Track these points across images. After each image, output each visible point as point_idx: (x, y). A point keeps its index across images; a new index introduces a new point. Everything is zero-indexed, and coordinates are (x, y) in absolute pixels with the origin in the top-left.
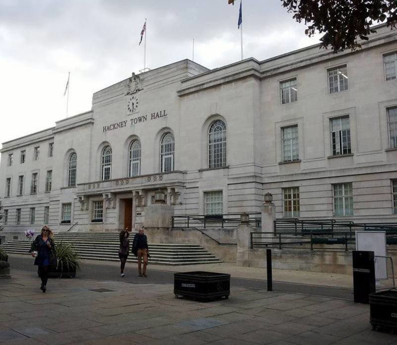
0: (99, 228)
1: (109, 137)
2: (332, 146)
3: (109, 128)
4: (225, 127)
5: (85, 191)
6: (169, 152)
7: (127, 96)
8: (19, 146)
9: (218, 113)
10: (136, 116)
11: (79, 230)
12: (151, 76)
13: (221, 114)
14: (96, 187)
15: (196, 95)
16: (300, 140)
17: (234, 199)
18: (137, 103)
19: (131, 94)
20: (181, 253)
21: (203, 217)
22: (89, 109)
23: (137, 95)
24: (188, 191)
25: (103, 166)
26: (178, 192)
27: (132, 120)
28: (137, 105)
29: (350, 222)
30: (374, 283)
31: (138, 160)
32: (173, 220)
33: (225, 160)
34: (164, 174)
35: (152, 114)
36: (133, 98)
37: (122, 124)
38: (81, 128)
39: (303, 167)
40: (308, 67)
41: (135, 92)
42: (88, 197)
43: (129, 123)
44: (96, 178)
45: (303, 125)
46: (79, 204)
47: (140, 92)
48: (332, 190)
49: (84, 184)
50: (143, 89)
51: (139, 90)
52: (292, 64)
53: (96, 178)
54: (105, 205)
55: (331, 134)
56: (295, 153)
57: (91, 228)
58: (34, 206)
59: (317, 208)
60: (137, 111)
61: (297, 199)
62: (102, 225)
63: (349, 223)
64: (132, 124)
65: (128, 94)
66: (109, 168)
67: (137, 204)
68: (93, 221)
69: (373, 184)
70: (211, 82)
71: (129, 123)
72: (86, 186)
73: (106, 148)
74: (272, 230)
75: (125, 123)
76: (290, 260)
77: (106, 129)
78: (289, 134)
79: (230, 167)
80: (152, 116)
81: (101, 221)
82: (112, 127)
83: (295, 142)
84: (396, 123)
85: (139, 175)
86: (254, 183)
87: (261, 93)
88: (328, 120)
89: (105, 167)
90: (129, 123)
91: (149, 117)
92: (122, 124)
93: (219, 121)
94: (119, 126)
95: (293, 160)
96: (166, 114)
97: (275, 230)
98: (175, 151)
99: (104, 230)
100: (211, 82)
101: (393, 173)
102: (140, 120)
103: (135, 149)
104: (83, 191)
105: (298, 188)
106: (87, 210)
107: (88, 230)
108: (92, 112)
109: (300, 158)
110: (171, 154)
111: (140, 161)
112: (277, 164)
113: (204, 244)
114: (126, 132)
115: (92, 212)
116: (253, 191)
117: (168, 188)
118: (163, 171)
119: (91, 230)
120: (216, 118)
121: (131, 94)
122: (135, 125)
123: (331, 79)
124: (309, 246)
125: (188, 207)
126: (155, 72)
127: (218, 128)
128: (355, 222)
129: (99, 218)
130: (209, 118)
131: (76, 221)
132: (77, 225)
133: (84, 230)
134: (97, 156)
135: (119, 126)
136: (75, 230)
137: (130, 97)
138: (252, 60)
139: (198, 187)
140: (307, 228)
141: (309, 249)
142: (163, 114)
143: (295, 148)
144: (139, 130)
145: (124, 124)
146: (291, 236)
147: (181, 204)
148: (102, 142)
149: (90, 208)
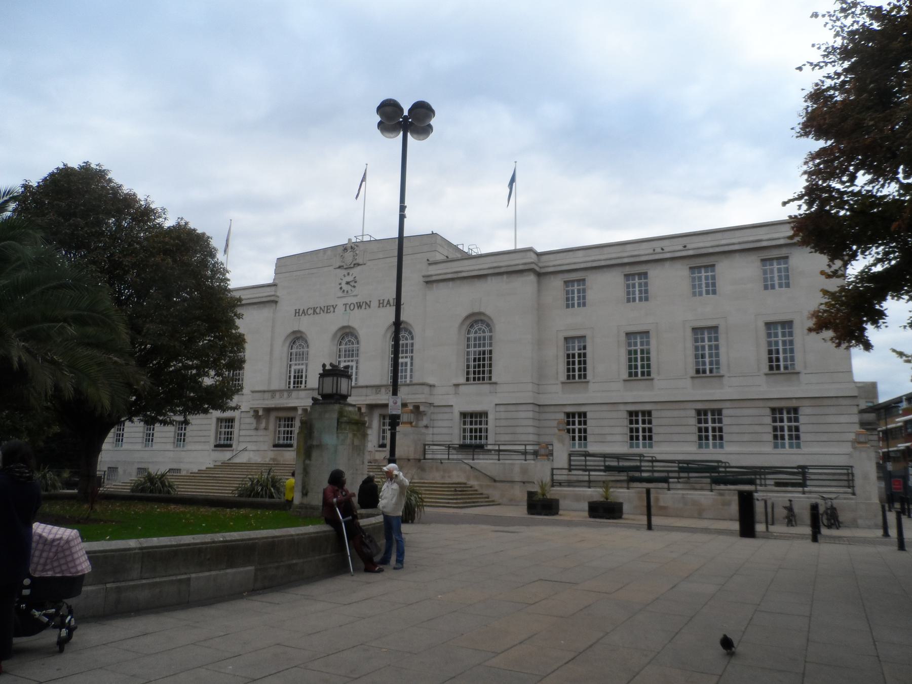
1: (305, 325)
2: (566, 369)
4: (308, 346)
6: (301, 362)
7: (339, 270)
9: (482, 310)
13: (488, 312)
15: (451, 284)
17: (503, 423)
19: (346, 268)
20: (195, 487)
21: (458, 446)
22: (271, 281)
23: (355, 271)
24: (436, 410)
26: (424, 411)
29: (652, 457)
32: (425, 449)
34: (292, 390)
36: (348, 274)
41: (352, 266)
43: (340, 309)
44: (278, 383)
49: (264, 392)
50: (365, 264)
51: (359, 265)
53: (278, 383)
55: (566, 355)
64: (346, 310)
65: (339, 267)
68: (275, 446)
69: (676, 413)
73: (297, 338)
74: (566, 466)
75: (334, 309)
80: (380, 304)
81: (231, 446)
82: (310, 311)
85: (408, 382)
86: (531, 405)
87: (539, 291)
88: (624, 335)
90: (340, 309)
91: (375, 304)
92: (328, 309)
93: (481, 320)
94: (323, 311)
96: (345, 306)
97: (570, 465)
101: (524, 405)
103: (298, 350)
106: (266, 429)
108: (273, 285)
110: (302, 364)
111: (307, 366)
113: (473, 483)
115: (275, 432)
116: (530, 415)
118: (292, 387)
119: (274, 460)
121: (346, 268)
123: (628, 286)
125: (436, 431)
126: (329, 252)
127: (480, 329)
128: (659, 457)
129: (226, 442)
130: (467, 317)
132: (246, 450)
135: (321, 308)
137: (342, 272)
138: (530, 250)
144: (355, 320)
146: (581, 472)
147: (426, 427)
148: (291, 331)
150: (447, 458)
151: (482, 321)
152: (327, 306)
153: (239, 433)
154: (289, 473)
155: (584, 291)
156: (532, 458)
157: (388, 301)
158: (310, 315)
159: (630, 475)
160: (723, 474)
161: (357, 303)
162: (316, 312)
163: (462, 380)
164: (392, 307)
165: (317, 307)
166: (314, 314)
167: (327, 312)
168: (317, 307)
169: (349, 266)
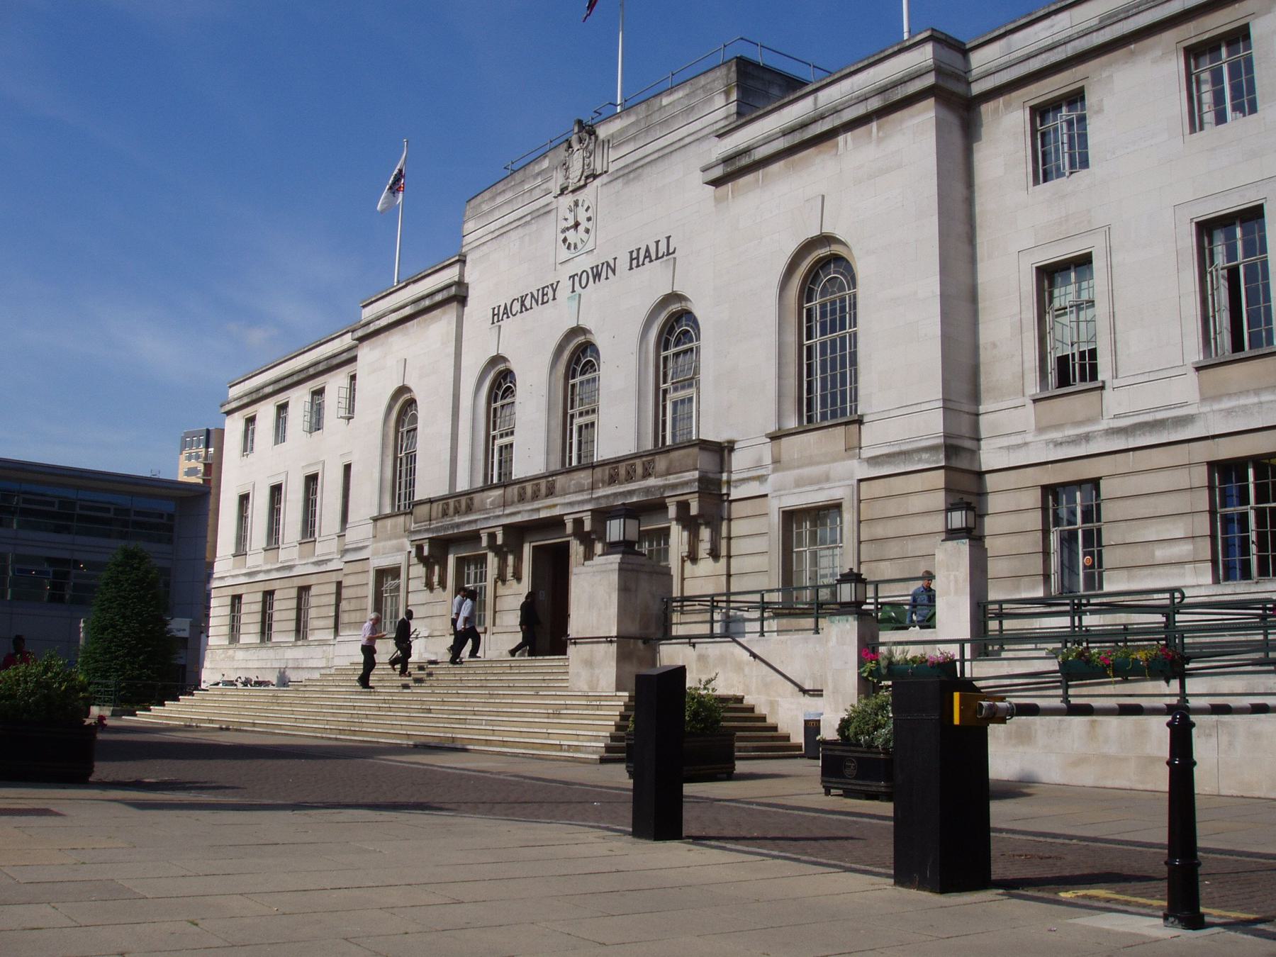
3: (507, 312)
10: (584, 263)
16: (1101, 309)
18: (589, 219)
23: (586, 196)
25: (494, 438)
27: (573, 277)
30: (1169, 884)
33: (855, 399)
35: (631, 253)
37: (544, 295)
40: (906, 51)
41: (582, 183)
45: (1110, 252)
48: (820, 557)
51: (595, 177)
58: (238, 591)
60: (590, 246)
61: (1095, 525)
64: (573, 291)
65: (563, 191)
71: (566, 285)
75: (554, 291)
77: (500, 315)
79: (865, 420)
80: (632, 259)
82: (517, 306)
89: (499, 442)
92: (544, 295)
94: (537, 302)
102: (597, 276)
105: (1095, 483)
120: (822, 252)
121: (573, 191)
135: (533, 296)
137: (568, 200)
139: (766, 496)
140: (1033, 646)
142: (663, 248)
150: (708, 632)
151: (837, 259)
152: (543, 288)
153: (414, 565)
154: (596, 738)
155: (1082, 119)
156: (747, 624)
157: (647, 250)
158: (515, 315)
159: (969, 658)
160: (1198, 651)
161: (592, 268)
162: (525, 307)
163: (792, 423)
164: (655, 262)
165: (527, 295)
166: (521, 312)
167: (543, 303)
168: (527, 295)
169: (578, 185)
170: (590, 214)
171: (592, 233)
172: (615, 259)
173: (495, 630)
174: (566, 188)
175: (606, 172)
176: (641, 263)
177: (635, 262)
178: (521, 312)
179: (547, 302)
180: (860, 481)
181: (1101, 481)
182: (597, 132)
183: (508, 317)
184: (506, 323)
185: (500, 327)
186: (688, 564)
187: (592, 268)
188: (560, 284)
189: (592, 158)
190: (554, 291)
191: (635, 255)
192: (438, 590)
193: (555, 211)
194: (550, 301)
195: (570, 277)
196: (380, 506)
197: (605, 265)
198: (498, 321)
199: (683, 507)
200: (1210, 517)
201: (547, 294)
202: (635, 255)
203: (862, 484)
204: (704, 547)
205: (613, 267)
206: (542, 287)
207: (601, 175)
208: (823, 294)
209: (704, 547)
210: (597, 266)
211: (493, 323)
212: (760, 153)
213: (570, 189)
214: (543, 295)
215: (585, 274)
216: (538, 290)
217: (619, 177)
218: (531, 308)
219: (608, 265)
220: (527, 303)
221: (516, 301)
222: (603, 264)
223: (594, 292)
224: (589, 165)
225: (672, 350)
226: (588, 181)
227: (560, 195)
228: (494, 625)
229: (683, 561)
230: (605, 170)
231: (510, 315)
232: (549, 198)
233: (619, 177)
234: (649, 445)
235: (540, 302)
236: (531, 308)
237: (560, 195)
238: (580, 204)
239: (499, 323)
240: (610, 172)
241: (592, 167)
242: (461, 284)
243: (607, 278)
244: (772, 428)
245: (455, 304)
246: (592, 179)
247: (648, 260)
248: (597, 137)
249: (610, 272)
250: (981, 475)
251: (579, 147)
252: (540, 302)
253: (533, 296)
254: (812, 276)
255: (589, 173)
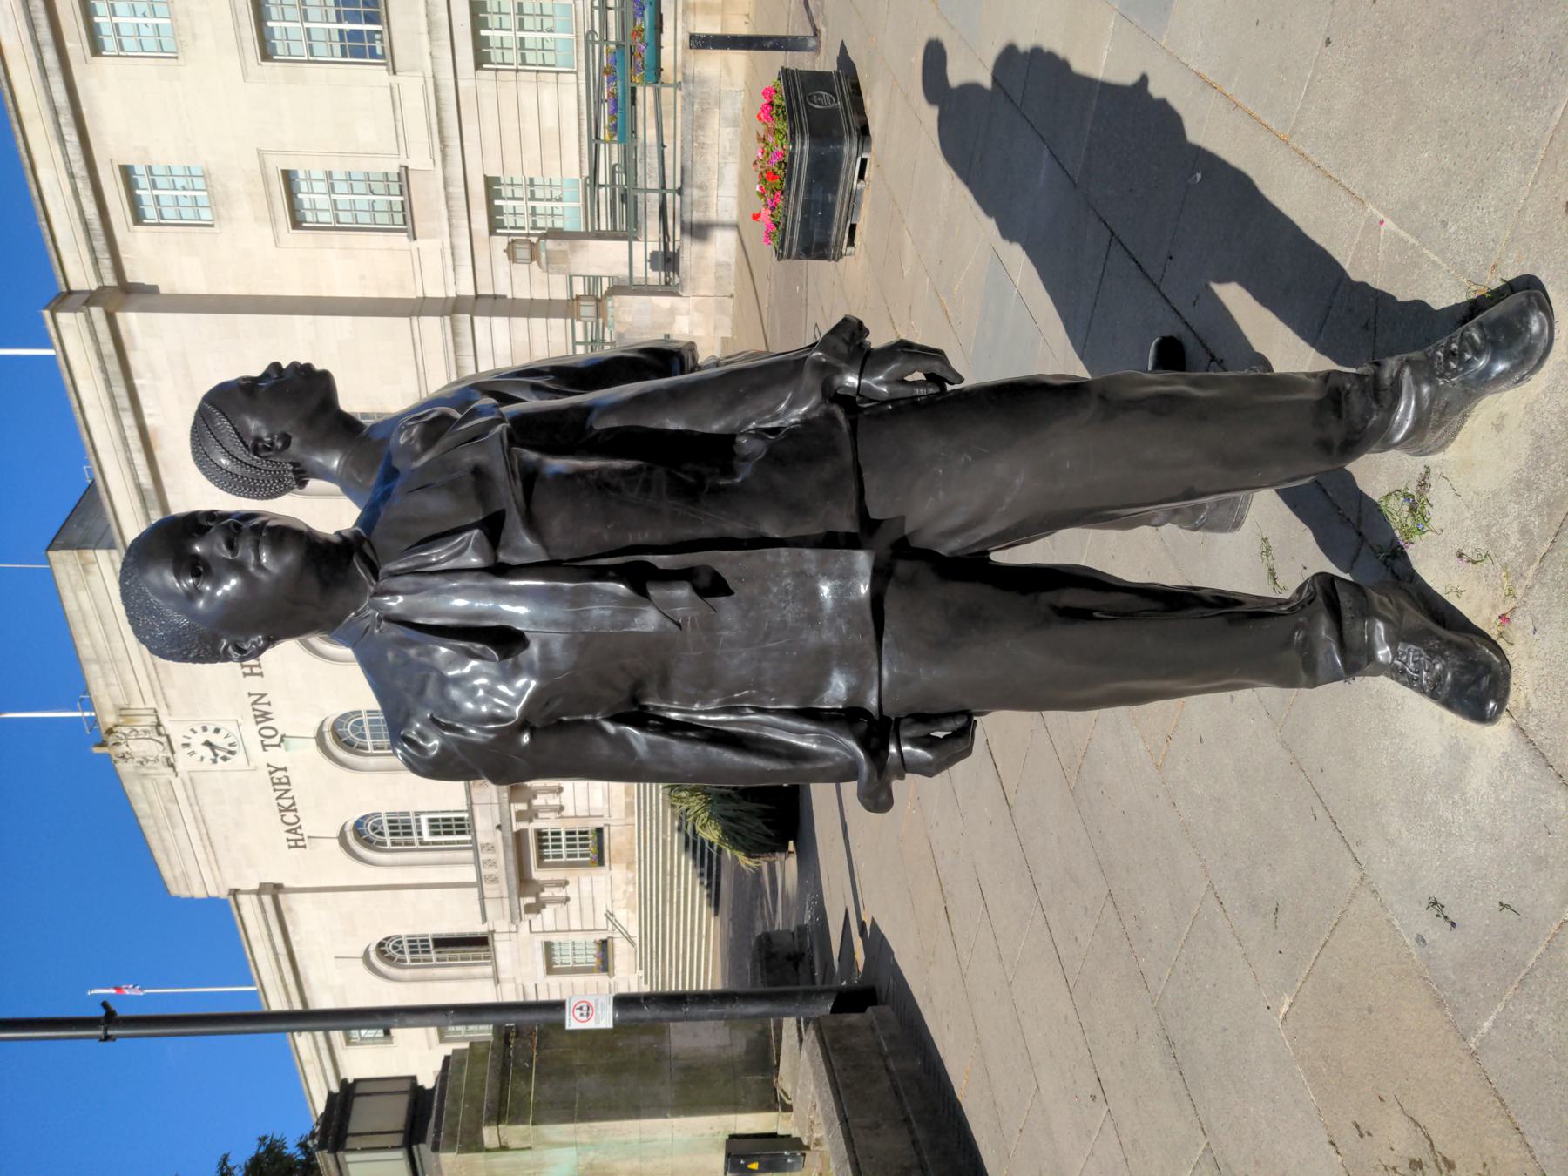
0: (617, 840)
3: (294, 829)
5: (505, 894)
7: (179, 767)
8: (96, 225)
10: (251, 731)
11: (628, 906)
12: (108, 685)
14: (492, 871)
18: (205, 729)
25: (421, 843)
27: (264, 746)
28: (211, 728)
31: (418, 821)
35: (290, 847)
36: (186, 745)
37: (280, 781)
38: (290, 929)
39: (421, 158)
41: (164, 739)
42: (524, 882)
46: (548, 912)
47: (163, 722)
51: (159, 724)
52: (72, 176)
54: (546, 823)
56: (379, 187)
57: (624, 865)
59: (550, 121)
60: (232, 728)
62: (613, 829)
63: (596, 13)
66: (431, 820)
67: (552, 815)
70: (130, 462)
72: (487, 894)
75: (277, 769)
76: (709, 157)
78: (314, 198)
81: (599, 831)
82: (290, 817)
83: (341, 187)
84: (304, 3)
89: (427, 837)
90: (277, 757)
92: (280, 781)
94: (287, 791)
95: (401, 194)
98: (412, 809)
99: (630, 820)
100: (130, 462)
102: (265, 716)
104: (506, 902)
107: (630, 875)
109: (393, 168)
112: (414, 244)
114: (304, 760)
117: (515, 830)
120: (328, 737)
121: (173, 752)
122: (281, 733)
124: (667, 93)
131: (602, 922)
133: (631, 889)
134: (388, 867)
135: (279, 797)
136: (629, 919)
137: (181, 758)
139: (536, 986)
141: (678, 92)
143: (360, 187)
145: (279, 774)
149: (559, 874)
152: (274, 784)
157: (289, 831)
166: (295, 810)
167: (289, 783)
168: (279, 805)
169: (166, 744)
170: (198, 728)
171: (219, 725)
172: (250, 695)
173: (606, 816)
174: (168, 759)
175: (156, 711)
176: (300, 837)
177: (300, 843)
178: (295, 810)
179: (288, 778)
180: (531, 931)
181: (488, 175)
182: (110, 726)
183: (300, 827)
184: (307, 829)
185: (309, 837)
186: (564, 813)
187: (258, 723)
188: (271, 764)
189: (139, 729)
190: (277, 769)
191: (293, 843)
192: (571, 891)
193: (192, 774)
194: (287, 774)
195: (265, 750)
196: (485, 977)
197: (256, 707)
198: (303, 840)
199: (521, 816)
200: (534, 317)
201: (280, 779)
202: (293, 843)
203: (533, 930)
204: (558, 892)
205: (257, 697)
206: (270, 783)
207: (158, 718)
208: (363, 736)
209: (558, 892)
210: (256, 717)
211: (304, 847)
212: (146, 480)
213: (169, 754)
214: (280, 783)
215: (264, 732)
216: (275, 790)
217: (163, 694)
218: (293, 798)
219: (255, 703)
220: (286, 803)
221: (284, 818)
222: (254, 710)
223: (281, 722)
224: (145, 732)
225: (408, 956)
226: (163, 732)
227: (175, 770)
228: (602, 816)
229: (562, 817)
230: (152, 712)
231: (297, 825)
232: (176, 782)
233: (163, 694)
234: (469, 855)
235: (286, 787)
236: (293, 798)
237: (175, 770)
238: (187, 741)
239: (306, 838)
240: (155, 706)
241: (148, 728)
242: (260, 891)
243: (269, 704)
244: (491, 983)
245: (281, 897)
246: (161, 729)
247: (299, 831)
248: (116, 726)
249: (263, 700)
250: (477, 296)
251: (124, 745)
252: (286, 787)
253: (279, 797)
254: (348, 745)
255: (155, 731)
